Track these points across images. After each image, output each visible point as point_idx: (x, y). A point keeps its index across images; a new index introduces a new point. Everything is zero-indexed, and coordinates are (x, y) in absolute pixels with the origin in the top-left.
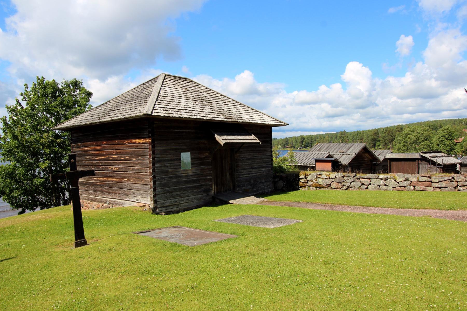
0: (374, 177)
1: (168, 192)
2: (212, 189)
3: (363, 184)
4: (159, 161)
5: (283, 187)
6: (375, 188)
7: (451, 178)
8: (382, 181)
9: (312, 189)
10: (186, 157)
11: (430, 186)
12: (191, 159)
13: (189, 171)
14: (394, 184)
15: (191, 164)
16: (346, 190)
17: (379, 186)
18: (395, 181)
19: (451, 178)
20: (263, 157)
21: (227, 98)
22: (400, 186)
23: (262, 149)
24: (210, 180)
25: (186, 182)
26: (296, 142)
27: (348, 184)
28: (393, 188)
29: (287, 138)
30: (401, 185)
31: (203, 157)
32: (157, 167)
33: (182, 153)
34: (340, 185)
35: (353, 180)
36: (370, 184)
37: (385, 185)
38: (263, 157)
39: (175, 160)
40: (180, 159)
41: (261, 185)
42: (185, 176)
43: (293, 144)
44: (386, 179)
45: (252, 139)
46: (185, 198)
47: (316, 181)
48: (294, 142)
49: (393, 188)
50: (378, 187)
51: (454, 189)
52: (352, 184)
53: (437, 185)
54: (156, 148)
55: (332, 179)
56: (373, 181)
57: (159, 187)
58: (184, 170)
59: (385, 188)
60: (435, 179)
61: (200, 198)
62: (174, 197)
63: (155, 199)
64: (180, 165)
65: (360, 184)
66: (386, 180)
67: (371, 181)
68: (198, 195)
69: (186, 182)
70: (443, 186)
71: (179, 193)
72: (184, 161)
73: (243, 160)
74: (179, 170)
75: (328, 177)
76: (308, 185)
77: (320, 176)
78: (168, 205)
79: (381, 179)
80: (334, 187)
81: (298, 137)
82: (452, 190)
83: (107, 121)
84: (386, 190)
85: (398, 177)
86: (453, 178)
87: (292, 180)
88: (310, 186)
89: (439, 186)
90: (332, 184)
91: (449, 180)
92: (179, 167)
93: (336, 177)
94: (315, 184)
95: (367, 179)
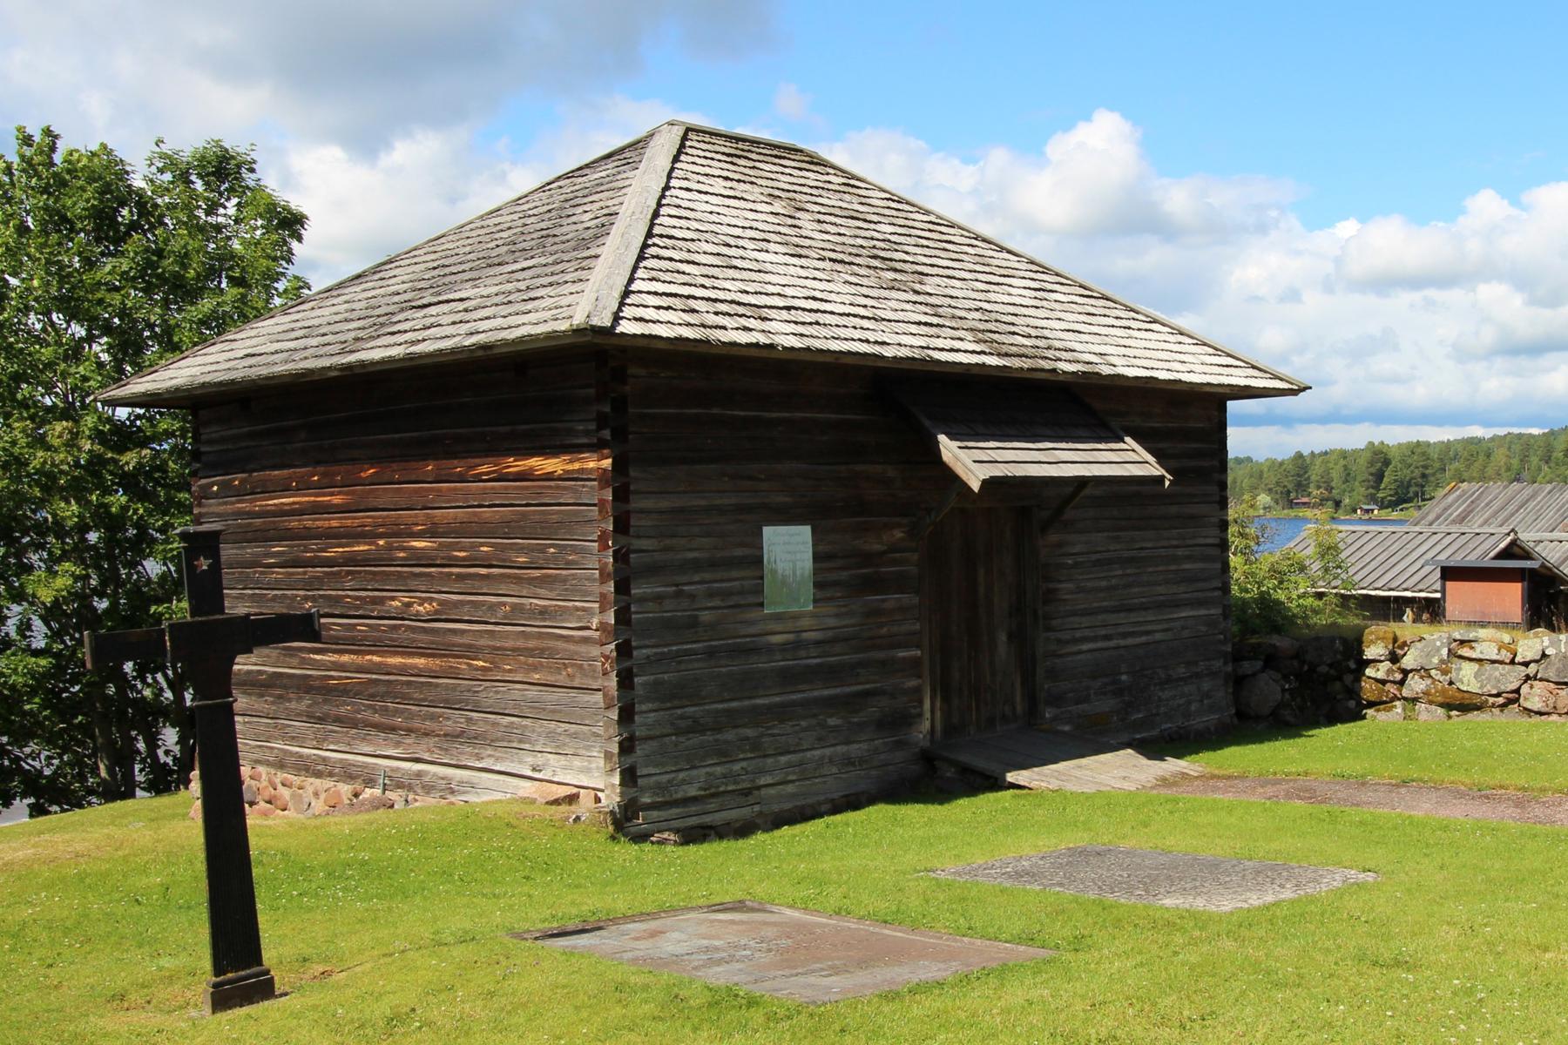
2: (920, 715)
10: (789, 549)
13: (805, 623)
15: (818, 585)
20: (1180, 552)
23: (1174, 510)
25: (789, 678)
26: (1348, 477)
29: (1299, 456)
31: (877, 547)
32: (642, 600)
33: (768, 532)
38: (1180, 552)
39: (731, 563)
42: (783, 647)
43: (1330, 489)
45: (1128, 460)
46: (783, 759)
47: (1445, 672)
48: (1336, 475)
54: (636, 503)
55: (1526, 664)
57: (648, 699)
64: (759, 590)
68: (848, 742)
69: (789, 678)
71: (749, 732)
73: (1076, 565)
74: (752, 615)
76: (1405, 693)
77: (1465, 652)
80: (1535, 703)
93: (1544, 655)
94: (1444, 691)
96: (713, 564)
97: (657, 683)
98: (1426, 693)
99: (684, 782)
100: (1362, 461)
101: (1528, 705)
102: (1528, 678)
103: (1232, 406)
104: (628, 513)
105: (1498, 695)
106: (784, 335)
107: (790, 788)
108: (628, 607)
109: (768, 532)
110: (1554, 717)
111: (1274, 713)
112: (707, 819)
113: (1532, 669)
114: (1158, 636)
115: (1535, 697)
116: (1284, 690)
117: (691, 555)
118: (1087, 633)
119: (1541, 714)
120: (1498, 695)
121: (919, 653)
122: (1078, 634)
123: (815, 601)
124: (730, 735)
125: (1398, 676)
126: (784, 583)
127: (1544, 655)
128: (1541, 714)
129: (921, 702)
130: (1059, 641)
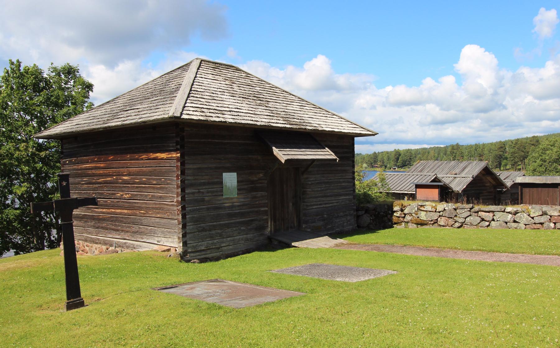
1: (204, 230)
2: (268, 226)
4: (192, 185)
6: (500, 225)
8: (510, 215)
9: (410, 227)
10: (230, 179)
12: (238, 182)
13: (235, 200)
14: (527, 219)
15: (238, 189)
16: (459, 227)
17: (506, 223)
18: (529, 215)
20: (341, 180)
22: (535, 223)
23: (339, 168)
24: (265, 213)
25: (230, 216)
26: (389, 159)
27: (462, 220)
28: (526, 225)
29: (375, 153)
30: (537, 221)
31: (255, 179)
32: (189, 194)
33: (224, 174)
34: (451, 222)
35: (468, 213)
36: (493, 220)
37: (515, 221)
38: (341, 180)
39: (214, 183)
40: (221, 183)
42: (229, 207)
43: (383, 162)
44: (516, 213)
45: (327, 154)
46: (229, 239)
47: (416, 214)
49: (526, 225)
52: (468, 219)
54: (187, 166)
55: (439, 212)
57: (191, 222)
58: (227, 199)
63: (185, 239)
64: (222, 191)
66: (515, 215)
67: (494, 215)
69: (230, 216)
71: (219, 231)
73: (312, 184)
74: (220, 198)
76: (405, 220)
77: (422, 209)
79: (509, 213)
80: (442, 223)
81: (391, 152)
84: (516, 228)
85: (533, 211)
88: (408, 222)
92: (219, 194)
93: (445, 210)
96: (209, 184)
100: (393, 155)
101: (440, 224)
103: (356, 138)
104: (184, 169)
105: (432, 221)
107: (231, 247)
108: (185, 196)
109: (224, 174)
110: (447, 227)
113: (441, 213)
115: (442, 221)
117: (202, 181)
119: (444, 226)
120: (432, 221)
125: (403, 216)
127: (445, 210)
128: (444, 226)
129: (268, 223)
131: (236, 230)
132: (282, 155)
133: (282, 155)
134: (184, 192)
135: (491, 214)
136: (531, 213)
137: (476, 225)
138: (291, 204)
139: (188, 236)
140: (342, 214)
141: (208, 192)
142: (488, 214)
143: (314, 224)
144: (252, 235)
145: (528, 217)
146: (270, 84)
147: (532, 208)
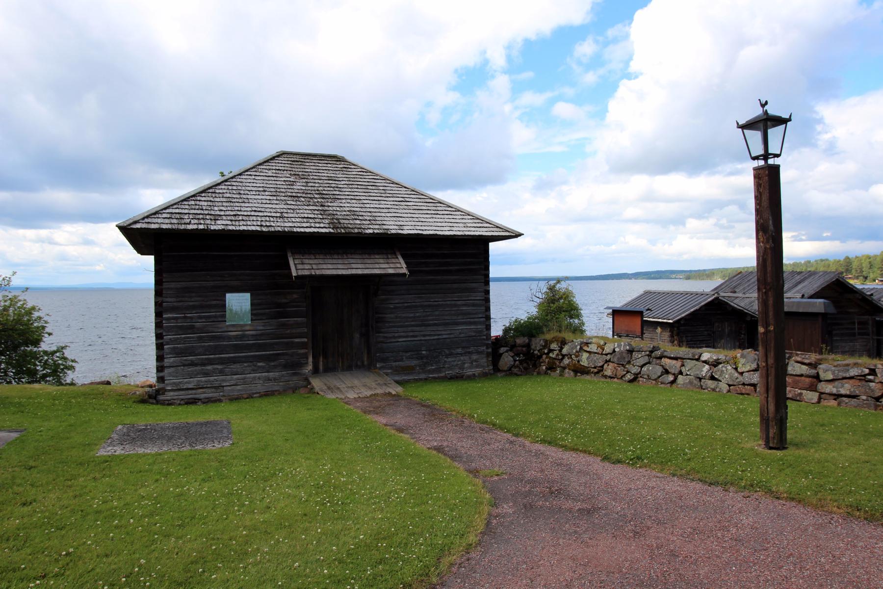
0: (690, 356)
1: (193, 364)
2: (307, 363)
3: (667, 372)
4: (173, 309)
5: (513, 366)
6: (691, 383)
7: (867, 371)
8: (707, 367)
9: (567, 375)
10: (239, 303)
11: (812, 388)
12: (252, 304)
13: (248, 328)
14: (731, 376)
15: (252, 314)
16: (631, 381)
17: (700, 379)
18: (736, 369)
19: (867, 371)
20: (459, 303)
21: (393, 183)
22: (744, 384)
23: (455, 286)
24: (303, 345)
25: (237, 348)
26: (871, 266)
27: (635, 370)
28: (730, 386)
29: (847, 258)
30: (747, 381)
31: (284, 301)
32: (168, 319)
33: (228, 295)
34: (621, 371)
35: (646, 359)
36: (681, 373)
37: (712, 378)
38: (459, 303)
39: (215, 306)
40: (225, 305)
41: (450, 359)
42: (236, 338)
43: (862, 271)
44: (716, 364)
45: (398, 266)
46: (235, 377)
47: (577, 357)
48: (865, 265)
49: (730, 386)
50: (696, 382)
51: (872, 402)
52: (645, 369)
53: (829, 388)
54: (165, 285)
55: (606, 355)
56: (689, 364)
57: (170, 354)
58: (233, 326)
59: (711, 384)
60: (826, 371)
61: (275, 379)
62: (206, 374)
63: (161, 374)
64: (224, 316)
65: (659, 370)
66: (715, 366)
67: (683, 365)
68: (268, 372)
69: (237, 348)
70: (843, 392)
71: (220, 367)
72: (234, 308)
73: (395, 308)
74: (221, 325)
75: (600, 351)
76: (562, 365)
77: (585, 348)
78: (191, 387)
79: (705, 362)
80: (608, 372)
81: (876, 256)
82: (869, 407)
83: (430, 235)
84: (714, 390)
85: (743, 361)
86: (873, 372)
87: (536, 352)
88: (564, 368)
89: (834, 391)
90: (605, 366)
91: (862, 378)
92: (220, 319)
93: (614, 351)
94: (575, 365)
95: (676, 359)
96: (201, 307)
97: (174, 348)
98: (568, 365)
99: (186, 383)
100: (878, 259)
101: (606, 373)
102: (607, 361)
103: (492, 245)
104: (162, 290)
105: (595, 368)
106: (252, 226)
107: (238, 387)
108: (161, 322)
109: (228, 295)
110: (616, 380)
111: (510, 369)
112: (197, 396)
113: (608, 357)
114: (445, 336)
115: (609, 370)
116: (515, 361)
117: (191, 304)
118: (402, 334)
119: (611, 378)
120: (595, 368)
121: (306, 340)
122: (396, 335)
123: (252, 320)
124: (209, 367)
125: (560, 357)
126: (236, 313)
127: (614, 351)
128: (611, 378)
129: (307, 358)
130: (386, 337)
131: (249, 366)
132: (300, 267)
133: (300, 267)
134: (161, 316)
135: (679, 363)
136: (740, 365)
137: (655, 380)
138: (357, 336)
139: (166, 371)
140: (459, 350)
141: (200, 317)
142: (674, 362)
143: (400, 363)
144: (277, 374)
145: (733, 371)
146: (377, 175)
147: (743, 356)
